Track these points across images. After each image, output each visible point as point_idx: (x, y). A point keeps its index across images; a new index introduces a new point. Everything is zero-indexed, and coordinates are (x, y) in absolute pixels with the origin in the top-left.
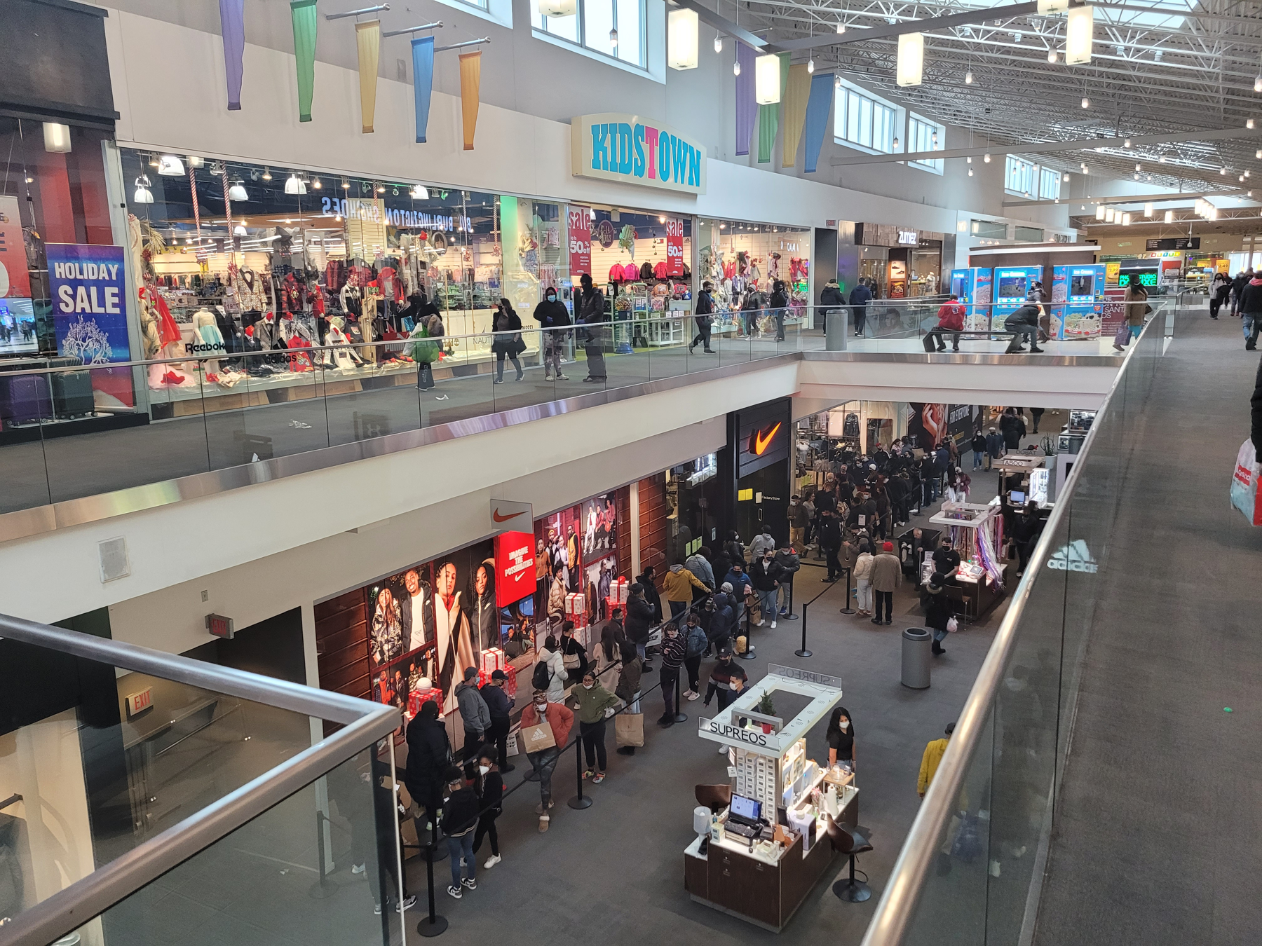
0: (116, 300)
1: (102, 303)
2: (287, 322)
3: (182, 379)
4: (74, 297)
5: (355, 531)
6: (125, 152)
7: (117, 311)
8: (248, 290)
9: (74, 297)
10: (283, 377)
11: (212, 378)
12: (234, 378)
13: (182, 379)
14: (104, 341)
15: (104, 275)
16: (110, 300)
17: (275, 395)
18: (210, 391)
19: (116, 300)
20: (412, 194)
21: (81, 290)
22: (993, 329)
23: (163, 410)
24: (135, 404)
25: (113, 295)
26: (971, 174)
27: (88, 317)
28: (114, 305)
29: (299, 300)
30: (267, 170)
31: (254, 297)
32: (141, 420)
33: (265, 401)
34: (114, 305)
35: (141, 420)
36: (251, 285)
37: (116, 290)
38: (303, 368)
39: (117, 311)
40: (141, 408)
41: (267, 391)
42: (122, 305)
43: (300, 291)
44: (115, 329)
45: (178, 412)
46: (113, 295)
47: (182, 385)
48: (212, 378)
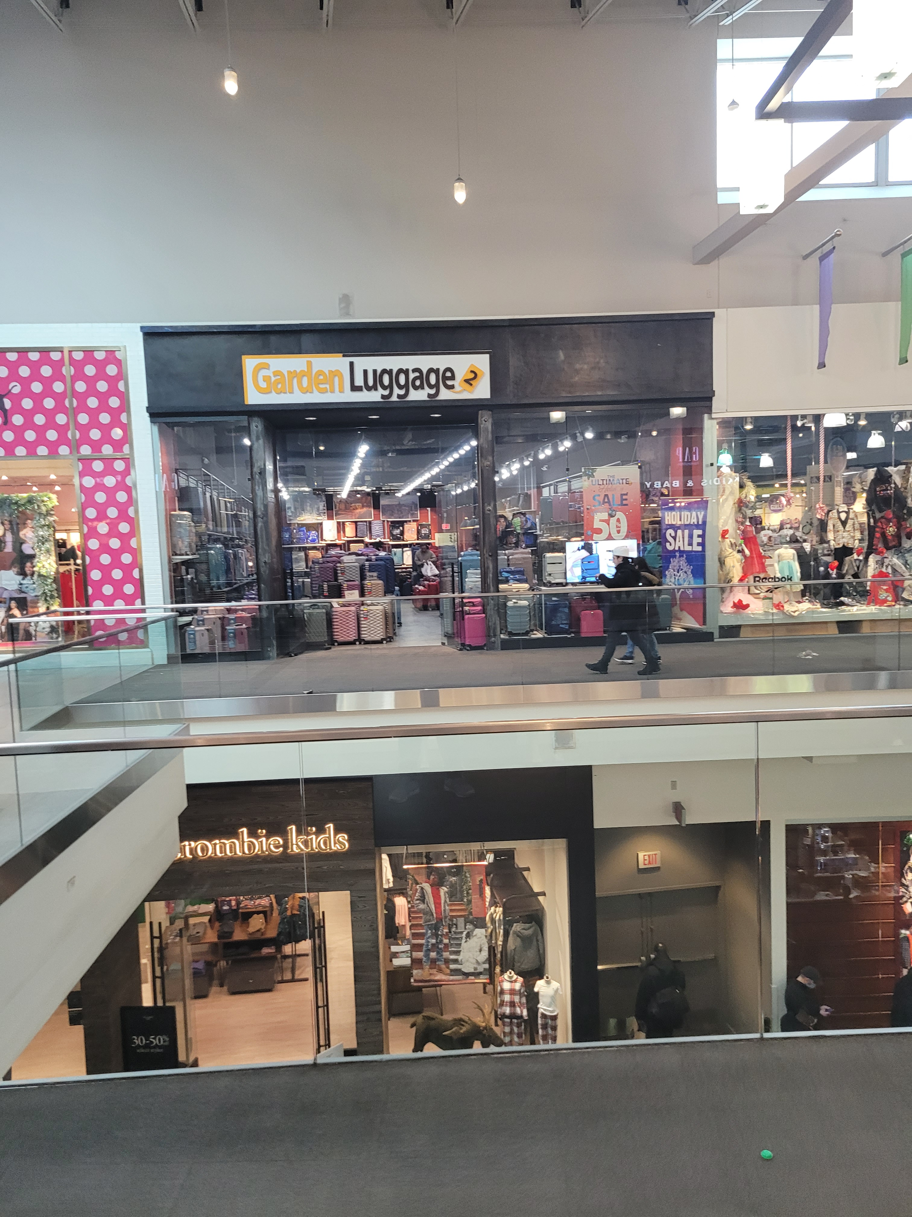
0: (700, 540)
1: (690, 544)
2: (879, 558)
3: (747, 606)
4: (674, 538)
5: (810, 759)
6: (733, 426)
7: (700, 549)
8: (841, 528)
9: (674, 538)
10: (855, 610)
11: (779, 606)
12: (805, 608)
13: (747, 606)
14: (689, 573)
15: (694, 521)
16: (696, 540)
17: (847, 626)
18: (778, 619)
19: (700, 540)
20: (767, 455)
21: (679, 532)
22: (302, 554)
23: (731, 631)
24: (704, 623)
25: (699, 536)
26: (801, 435)
27: (682, 552)
28: (699, 544)
29: (898, 536)
30: (862, 417)
31: (845, 534)
32: (707, 637)
33: (834, 631)
34: (699, 544)
35: (707, 637)
36: (844, 523)
37: (700, 532)
38: (883, 602)
39: (700, 549)
40: (711, 627)
41: (838, 623)
42: (702, 544)
43: (899, 527)
44: (697, 563)
45: (745, 634)
46: (699, 536)
47: (748, 611)
48: (779, 606)
